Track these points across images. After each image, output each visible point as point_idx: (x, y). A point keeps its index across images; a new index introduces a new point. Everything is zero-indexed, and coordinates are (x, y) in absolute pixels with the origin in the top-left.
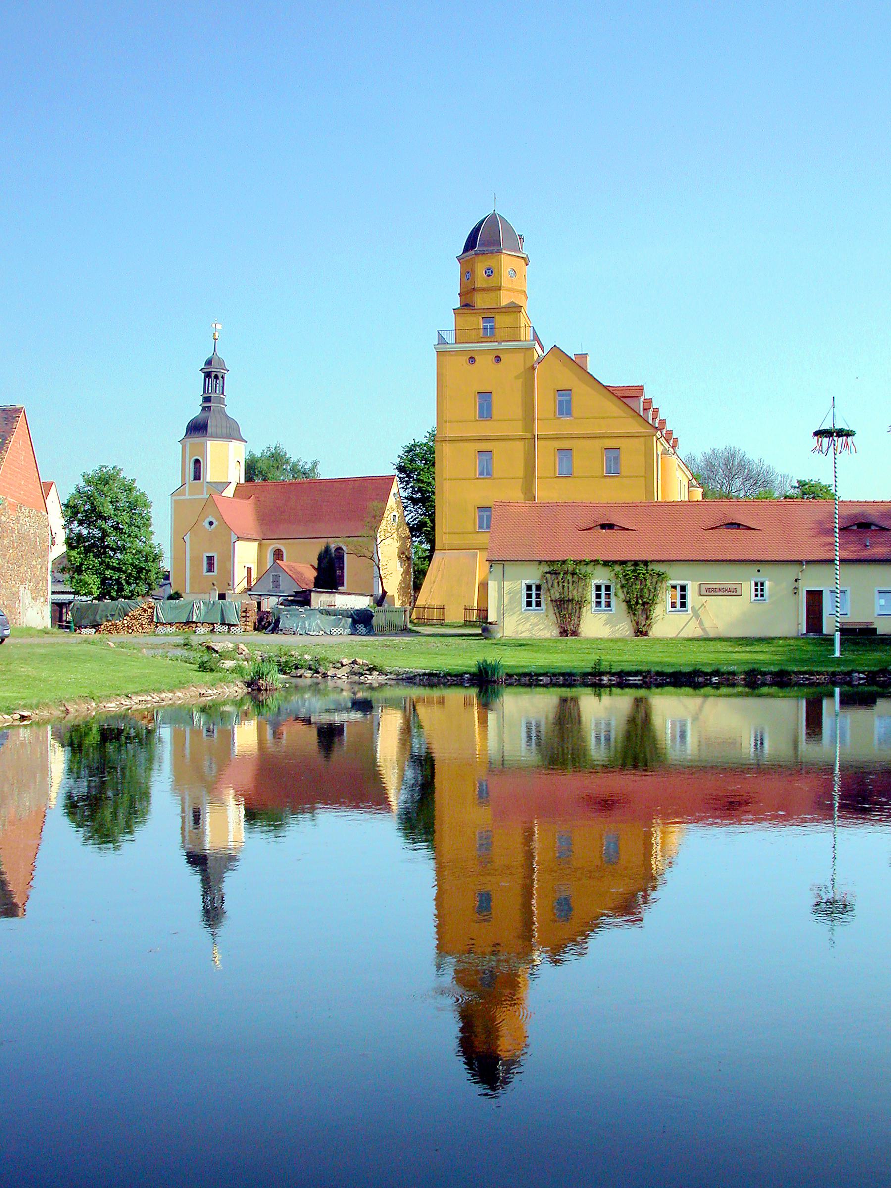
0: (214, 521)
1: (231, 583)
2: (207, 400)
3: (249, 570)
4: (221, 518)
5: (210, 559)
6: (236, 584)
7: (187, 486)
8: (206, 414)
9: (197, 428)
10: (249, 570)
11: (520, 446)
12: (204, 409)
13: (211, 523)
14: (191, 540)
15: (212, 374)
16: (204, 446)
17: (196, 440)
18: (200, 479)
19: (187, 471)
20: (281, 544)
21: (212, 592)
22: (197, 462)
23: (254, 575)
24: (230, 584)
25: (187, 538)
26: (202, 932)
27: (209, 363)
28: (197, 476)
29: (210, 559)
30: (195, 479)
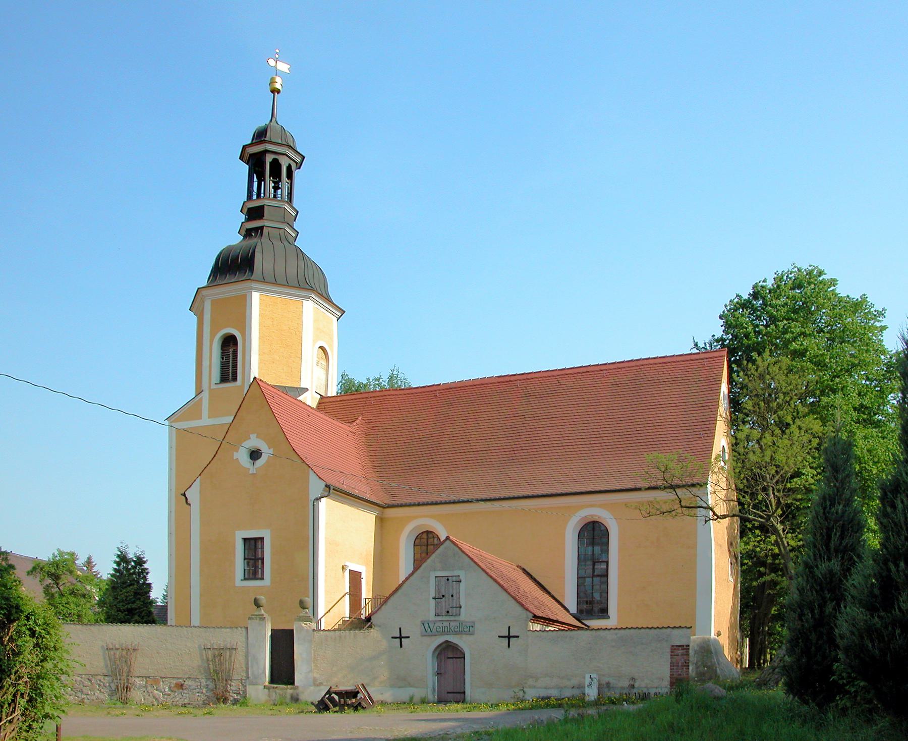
0: (260, 462)
1: (309, 600)
2: (254, 213)
3: (355, 578)
4: (281, 439)
5: (253, 546)
6: (321, 611)
7: (205, 395)
8: (251, 242)
9: (233, 266)
10: (355, 578)
11: (511, 639)
12: (248, 233)
13: (255, 455)
14: (203, 502)
15: (267, 162)
16: (244, 303)
17: (229, 290)
18: (235, 379)
19: (206, 363)
20: (432, 517)
21: (252, 624)
22: (229, 342)
23: (366, 592)
24: (306, 605)
25: (194, 495)
26: (301, 128)
27: (261, 135)
28: (229, 372)
29: (253, 546)
30: (224, 378)
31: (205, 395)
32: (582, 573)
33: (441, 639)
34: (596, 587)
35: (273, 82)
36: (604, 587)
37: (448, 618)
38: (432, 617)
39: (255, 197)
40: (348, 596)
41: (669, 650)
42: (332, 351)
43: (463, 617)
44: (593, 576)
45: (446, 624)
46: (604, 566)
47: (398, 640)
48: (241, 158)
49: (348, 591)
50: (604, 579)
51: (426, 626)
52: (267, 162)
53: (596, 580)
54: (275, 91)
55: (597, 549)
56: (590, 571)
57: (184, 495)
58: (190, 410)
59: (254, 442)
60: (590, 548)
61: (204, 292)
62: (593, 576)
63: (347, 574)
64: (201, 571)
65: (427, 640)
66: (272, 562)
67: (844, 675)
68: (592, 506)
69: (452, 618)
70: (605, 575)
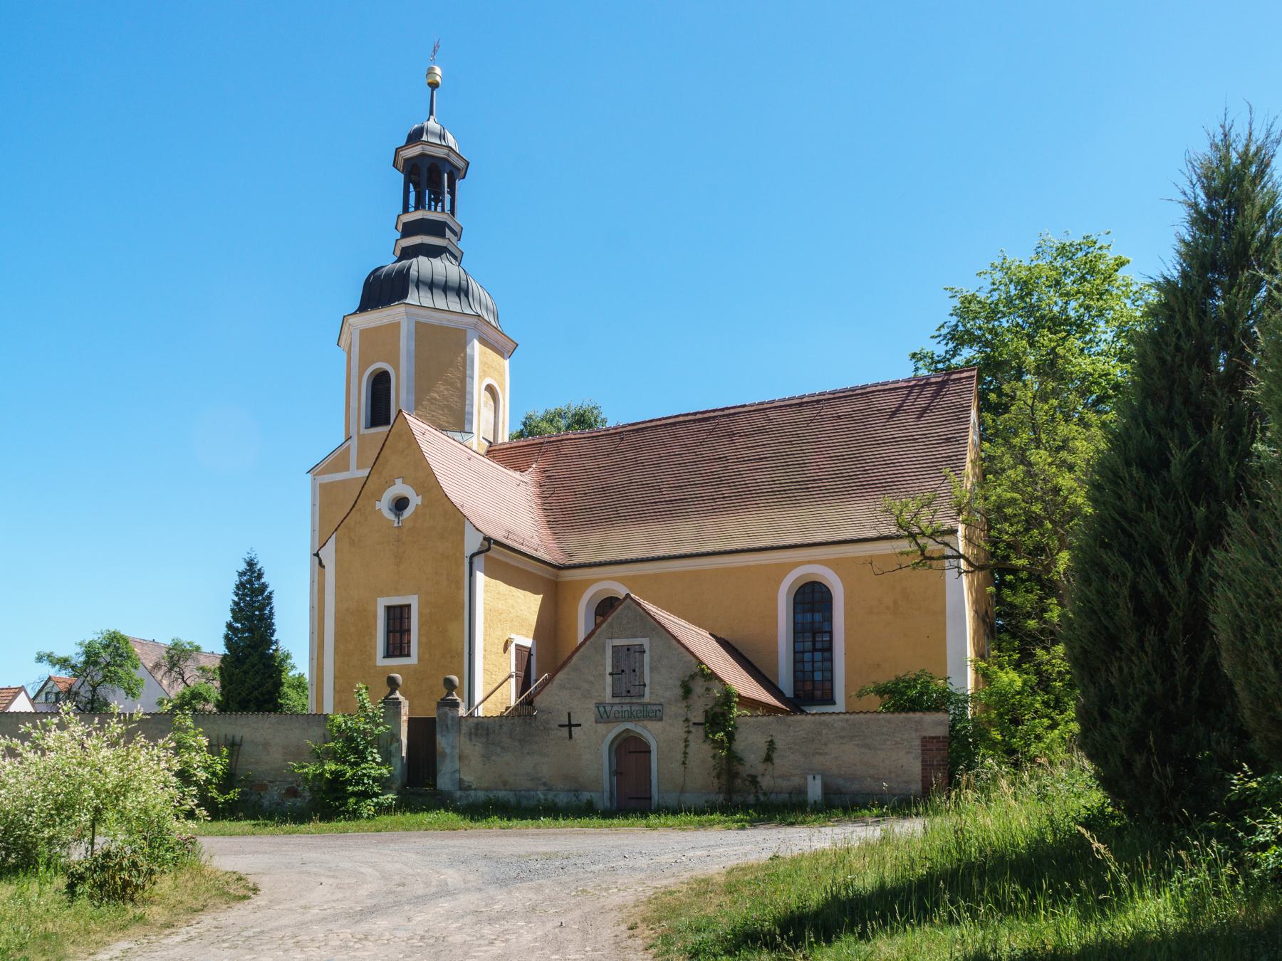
0: (408, 512)
5: (398, 617)
8: (405, 263)
15: (429, 175)
29: (398, 617)
31: (354, 443)
32: (800, 647)
33: (619, 728)
34: (818, 665)
35: (430, 72)
36: (827, 664)
37: (628, 700)
38: (608, 697)
39: (411, 209)
40: (513, 681)
41: (918, 742)
42: (503, 390)
43: (647, 699)
44: (814, 650)
45: (626, 708)
46: (827, 638)
47: (566, 729)
48: (395, 165)
49: (513, 669)
50: (827, 655)
51: (602, 709)
52: (429, 175)
53: (818, 656)
54: (434, 86)
55: (818, 617)
56: (808, 645)
57: (317, 555)
58: (337, 461)
59: (400, 489)
60: (809, 615)
61: (352, 320)
62: (814, 650)
63: (512, 649)
64: (336, 648)
65: (601, 728)
66: (420, 635)
67: (33, 769)
68: (810, 562)
69: (634, 700)
70: (829, 648)
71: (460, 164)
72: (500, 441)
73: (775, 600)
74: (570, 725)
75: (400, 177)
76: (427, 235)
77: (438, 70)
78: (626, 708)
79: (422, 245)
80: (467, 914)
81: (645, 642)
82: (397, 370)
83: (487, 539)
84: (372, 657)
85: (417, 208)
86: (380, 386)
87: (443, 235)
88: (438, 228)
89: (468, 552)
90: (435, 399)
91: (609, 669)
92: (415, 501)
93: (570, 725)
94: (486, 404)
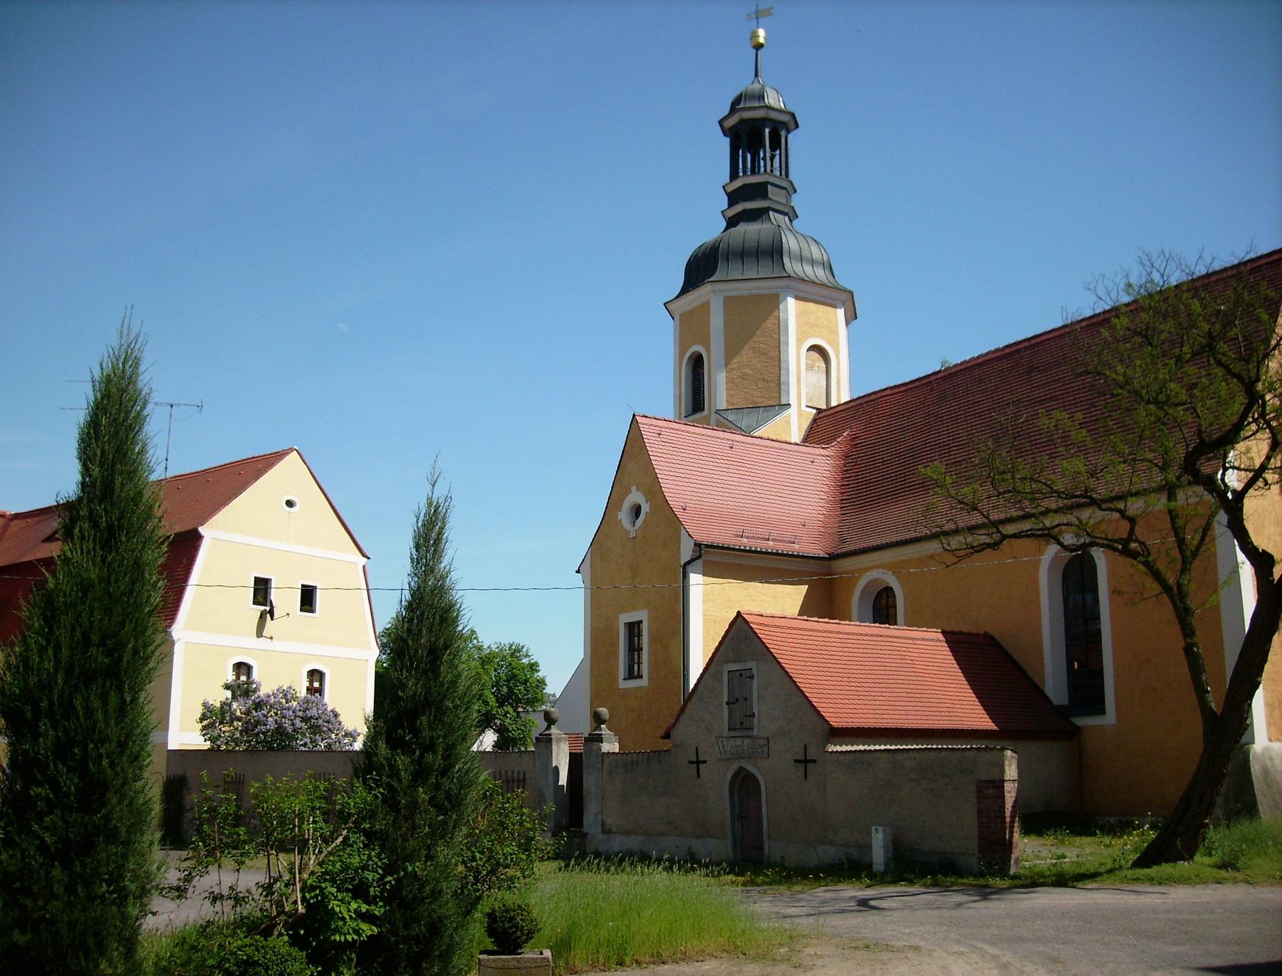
5: (633, 629)
15: (755, 135)
29: (633, 629)
33: (734, 767)
35: (754, 35)
52: (755, 135)
54: (759, 47)
71: (785, 118)
72: (834, 404)
73: (1035, 581)
74: (698, 762)
75: (727, 141)
76: (749, 200)
77: (761, 32)
78: (739, 742)
79: (744, 211)
80: (900, 950)
81: (751, 664)
82: (708, 350)
83: (698, 545)
84: (616, 680)
85: (753, 172)
86: (697, 364)
87: (765, 196)
88: (760, 191)
89: (684, 560)
90: (748, 375)
91: (726, 700)
92: (645, 508)
93: (698, 762)
94: (810, 368)
